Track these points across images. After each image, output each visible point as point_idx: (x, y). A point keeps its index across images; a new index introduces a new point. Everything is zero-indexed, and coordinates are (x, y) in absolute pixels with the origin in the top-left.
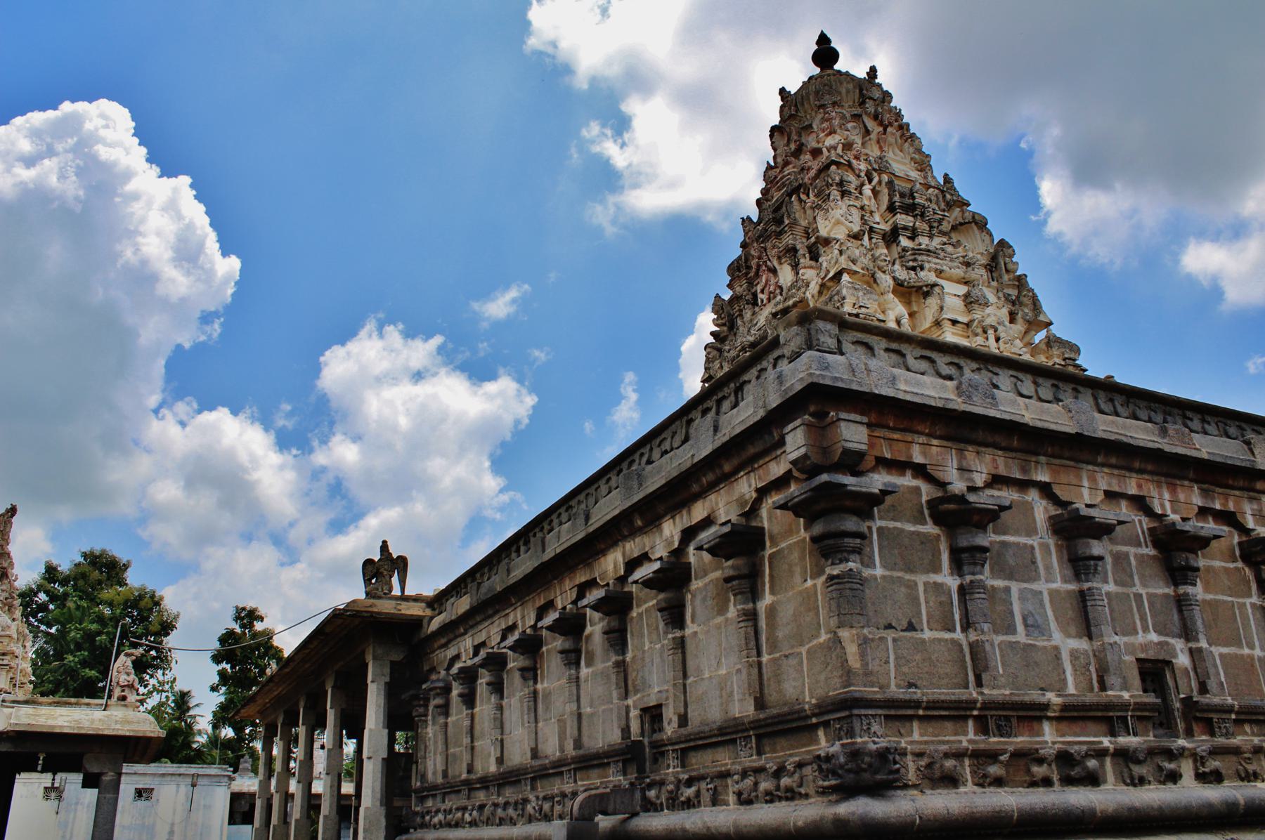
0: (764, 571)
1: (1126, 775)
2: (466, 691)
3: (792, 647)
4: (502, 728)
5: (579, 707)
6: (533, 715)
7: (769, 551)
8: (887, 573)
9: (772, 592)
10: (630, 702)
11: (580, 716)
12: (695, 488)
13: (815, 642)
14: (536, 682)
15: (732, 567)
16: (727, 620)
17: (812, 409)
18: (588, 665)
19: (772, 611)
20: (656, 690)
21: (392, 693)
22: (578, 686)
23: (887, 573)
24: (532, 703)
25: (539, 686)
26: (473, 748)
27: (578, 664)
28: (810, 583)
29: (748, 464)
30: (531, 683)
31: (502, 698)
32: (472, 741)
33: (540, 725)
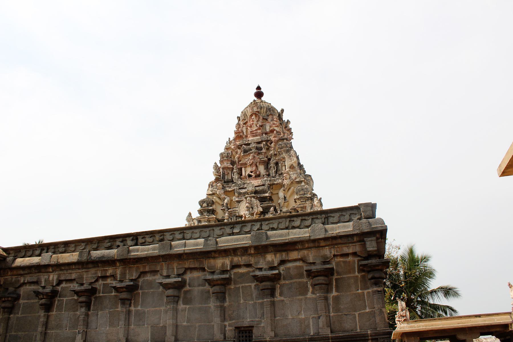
0: (332, 284)
1: (22, 272)
2: (49, 303)
3: (349, 312)
4: (87, 326)
5: (177, 322)
6: (127, 321)
7: (185, 289)
8: (334, 289)
9: (337, 291)
10: (227, 323)
11: (177, 326)
12: (63, 268)
13: (363, 311)
14: (130, 306)
15: (324, 280)
16: (306, 298)
17: (9, 273)
18: (185, 303)
19: (336, 299)
20: (248, 320)
21: (264, 193)
22: (177, 314)
23: (334, 289)
24: (127, 316)
25: (132, 308)
26: (45, 334)
27: (177, 302)
28: (360, 291)
29: (332, 246)
30: (128, 306)
31: (89, 309)
32: (46, 330)
33: (132, 327)
